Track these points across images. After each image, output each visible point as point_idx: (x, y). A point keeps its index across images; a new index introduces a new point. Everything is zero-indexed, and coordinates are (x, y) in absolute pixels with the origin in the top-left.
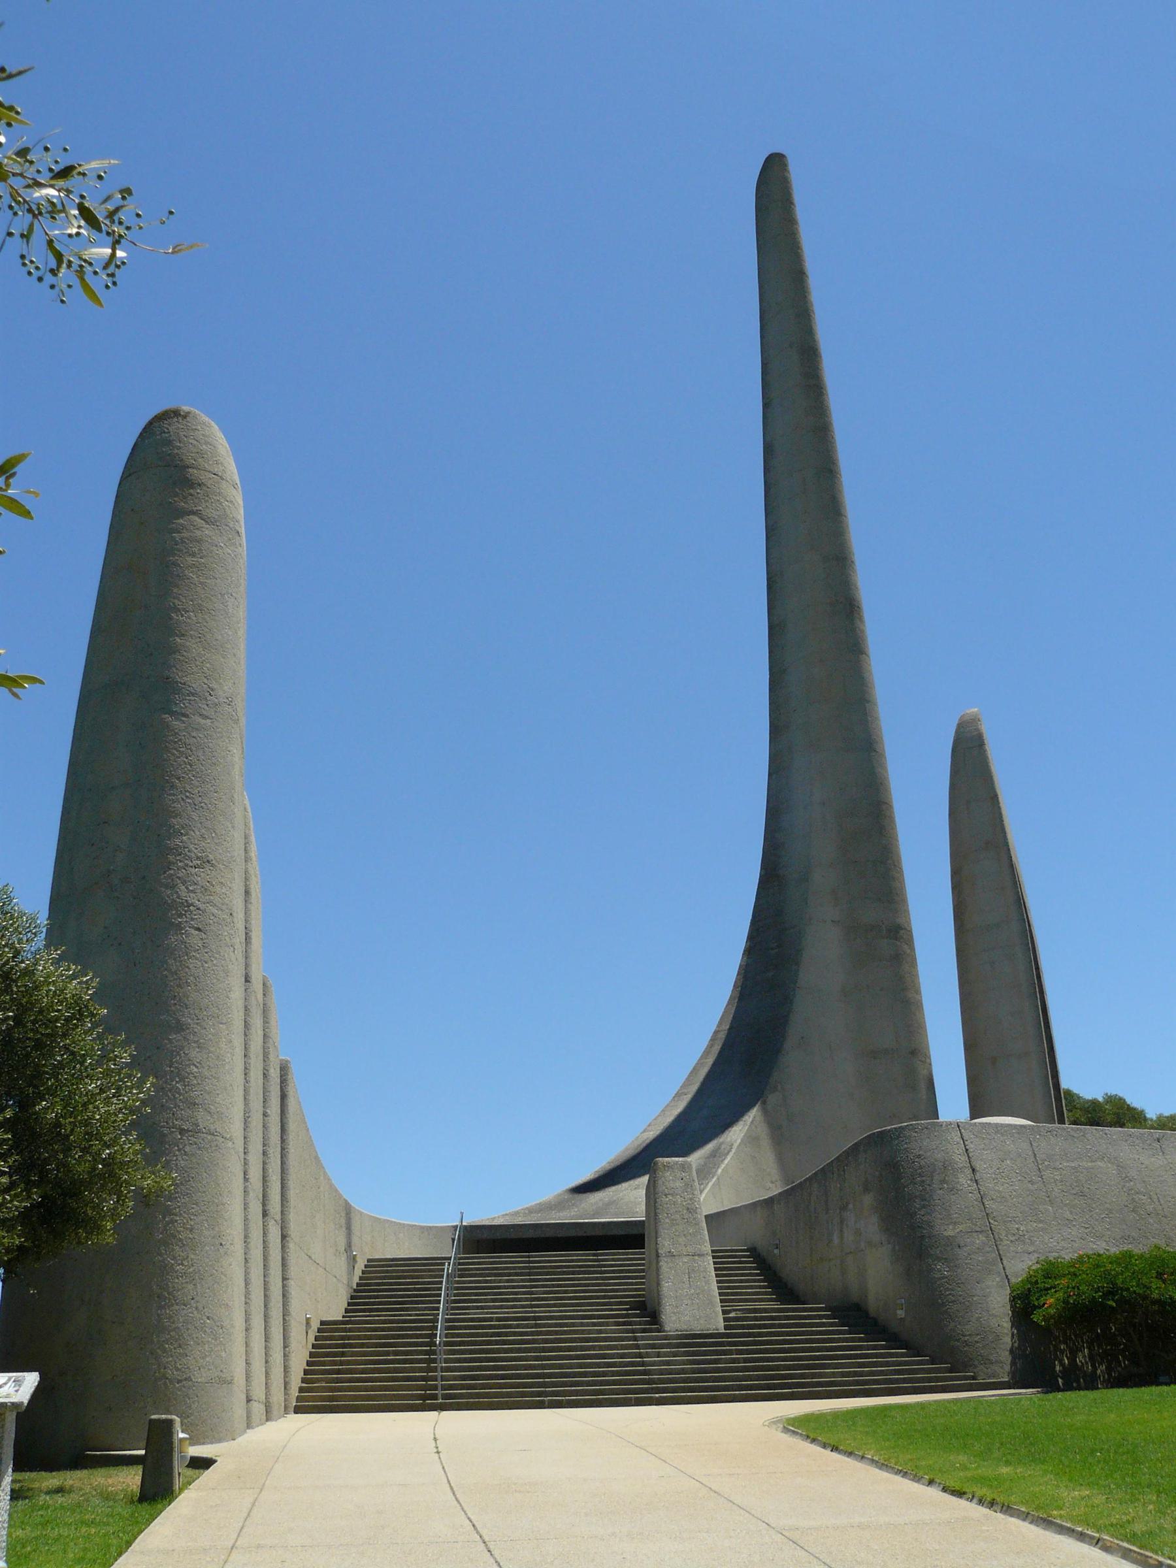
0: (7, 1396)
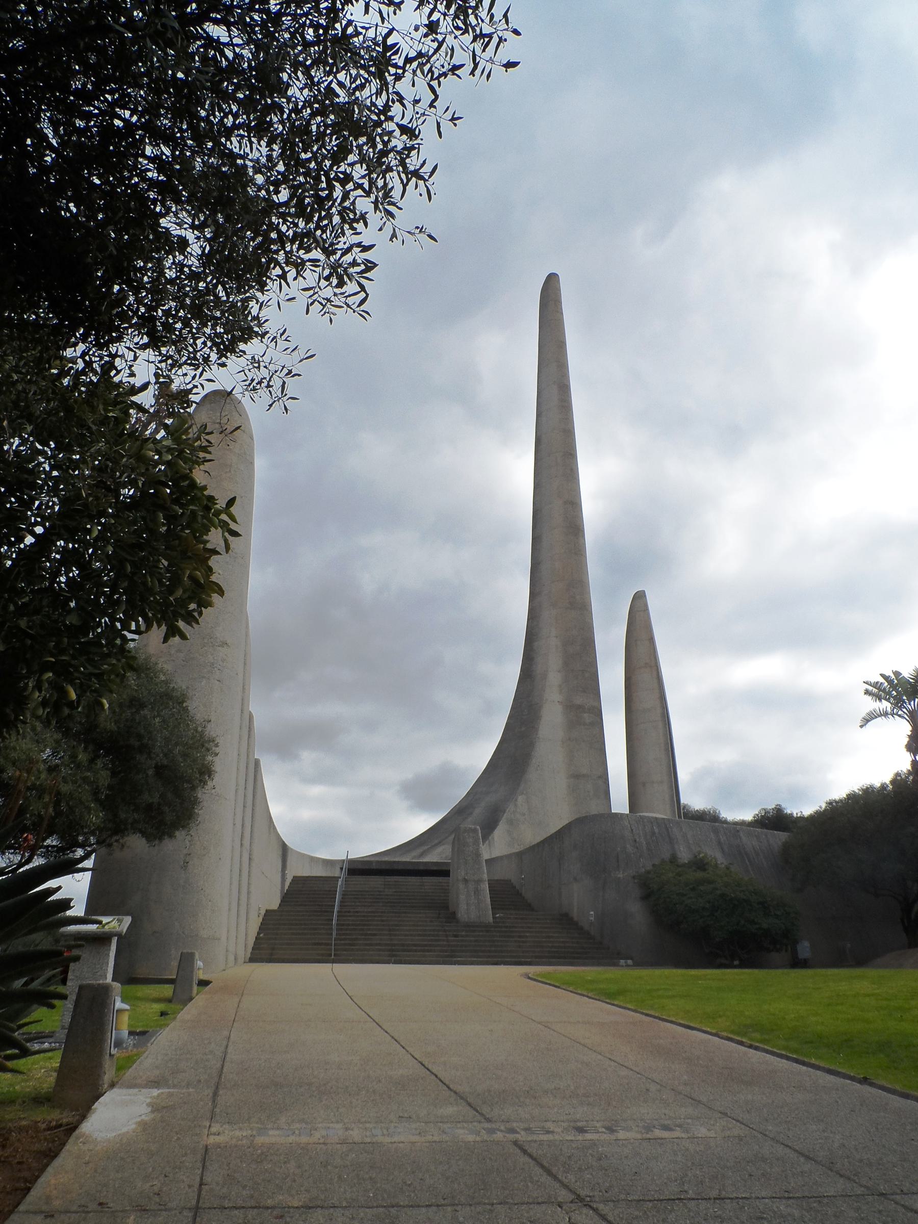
0: (114, 928)
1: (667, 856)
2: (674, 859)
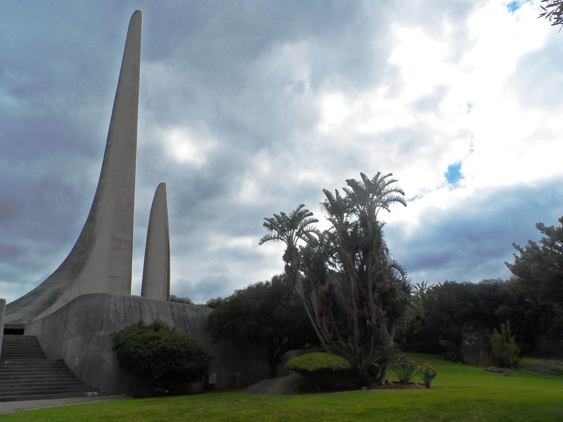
1: (136, 321)
2: (140, 324)
